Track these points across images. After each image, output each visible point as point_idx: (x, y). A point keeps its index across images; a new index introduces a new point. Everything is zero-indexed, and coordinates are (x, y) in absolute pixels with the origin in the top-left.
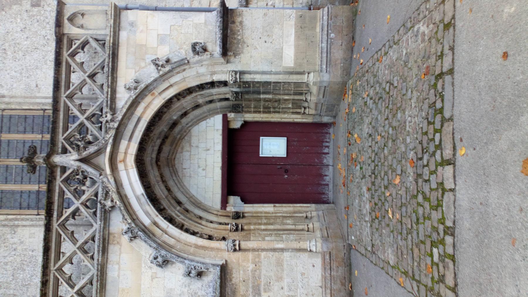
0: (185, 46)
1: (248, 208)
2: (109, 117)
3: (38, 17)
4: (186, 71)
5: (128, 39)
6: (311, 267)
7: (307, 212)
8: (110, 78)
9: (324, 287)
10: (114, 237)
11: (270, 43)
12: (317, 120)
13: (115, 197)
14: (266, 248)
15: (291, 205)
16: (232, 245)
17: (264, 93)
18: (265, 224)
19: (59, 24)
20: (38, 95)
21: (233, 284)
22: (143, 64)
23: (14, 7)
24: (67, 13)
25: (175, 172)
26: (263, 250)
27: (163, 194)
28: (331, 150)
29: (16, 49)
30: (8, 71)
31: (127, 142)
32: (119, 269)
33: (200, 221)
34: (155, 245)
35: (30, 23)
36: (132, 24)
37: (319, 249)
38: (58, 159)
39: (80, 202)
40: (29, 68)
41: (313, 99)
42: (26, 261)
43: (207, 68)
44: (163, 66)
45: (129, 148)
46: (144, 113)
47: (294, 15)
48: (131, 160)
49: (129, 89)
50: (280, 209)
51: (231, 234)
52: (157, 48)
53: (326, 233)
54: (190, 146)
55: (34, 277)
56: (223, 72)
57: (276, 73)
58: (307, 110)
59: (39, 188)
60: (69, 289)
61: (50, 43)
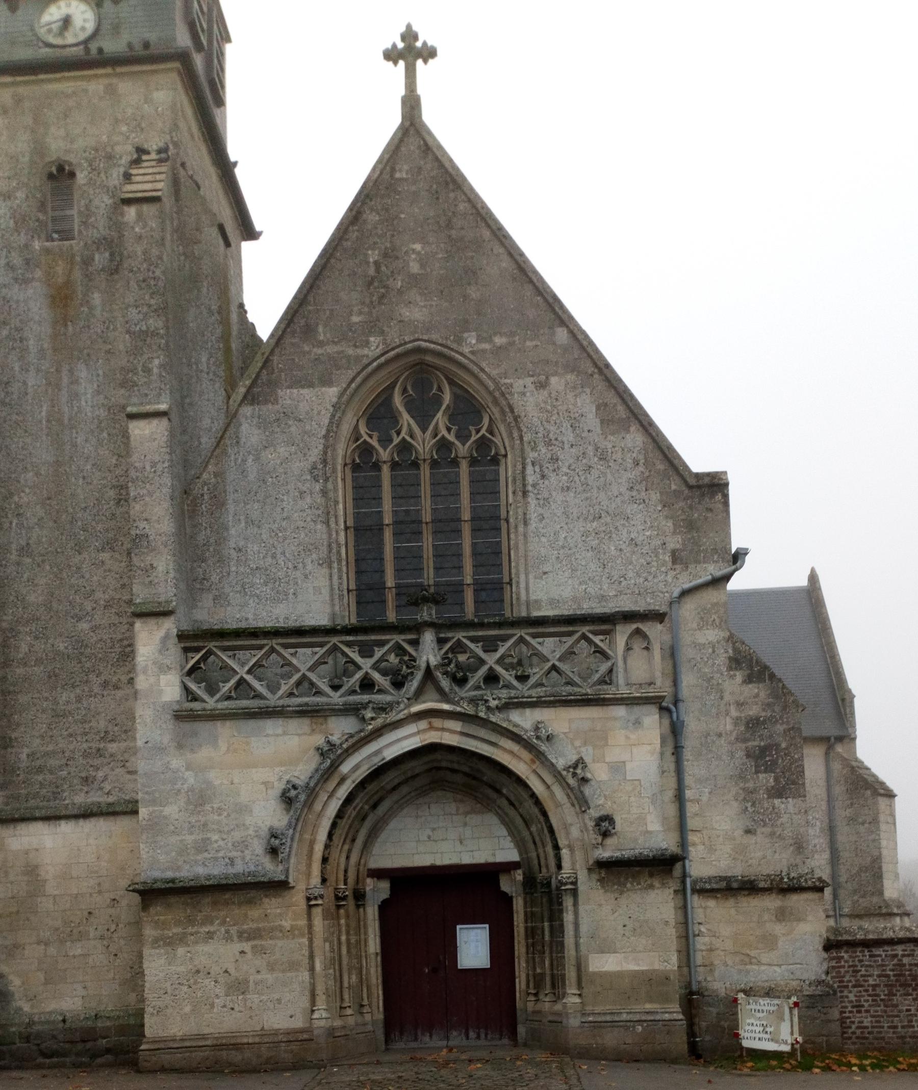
0: (609, 803)
1: (372, 913)
2: (493, 703)
3: (655, 564)
4: (572, 809)
5: (615, 719)
6: (290, 1013)
7: (371, 1007)
8: (552, 698)
9: (263, 1033)
10: (322, 724)
11: (622, 932)
12: (520, 1016)
13: (379, 722)
14: (314, 945)
15: (380, 981)
16: (316, 894)
17: (551, 927)
18: (348, 940)
19: (629, 617)
20: (531, 576)
21: (261, 899)
22: (578, 743)
23: (670, 524)
24: (645, 627)
25: (423, 792)
26: (311, 941)
27: (387, 783)
28: (473, 1043)
29: (602, 535)
30: (566, 527)
31: (459, 730)
32: (277, 735)
33: (348, 841)
34: (312, 784)
35: (645, 552)
36: (638, 723)
37: (317, 1024)
38: (428, 637)
39: (369, 671)
40: (573, 559)
41: (546, 1005)
42: (279, 585)
43: (578, 839)
44: (574, 775)
45: (450, 735)
46: (505, 750)
47: (669, 967)
48: (433, 737)
49: (537, 729)
50: (373, 964)
51: (331, 889)
52: (604, 762)
53: (339, 1034)
54: (466, 814)
55: (257, 601)
56: (573, 863)
57: (577, 945)
58: (532, 998)
59: (389, 588)
60: (247, 668)
61: (615, 586)
